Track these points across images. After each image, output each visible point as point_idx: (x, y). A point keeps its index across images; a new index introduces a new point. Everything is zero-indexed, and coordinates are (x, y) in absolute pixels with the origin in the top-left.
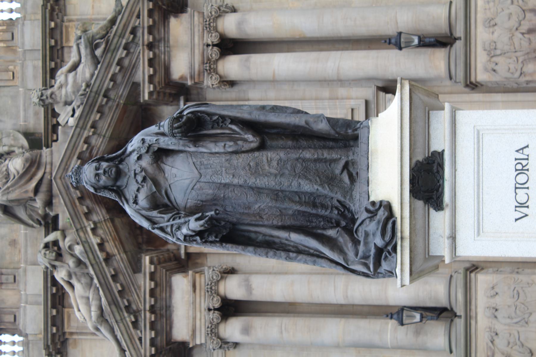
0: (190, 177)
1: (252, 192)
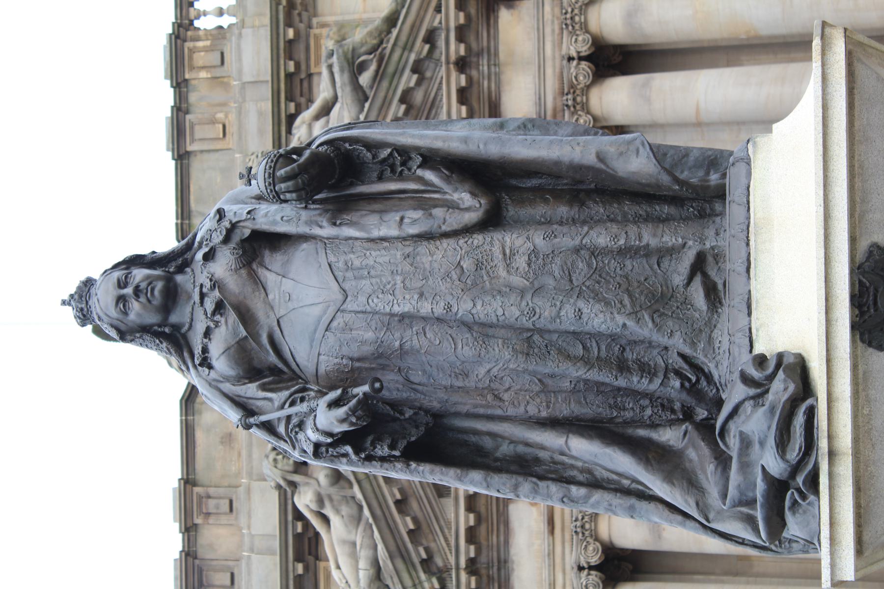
0: (321, 300)
1: (468, 335)
